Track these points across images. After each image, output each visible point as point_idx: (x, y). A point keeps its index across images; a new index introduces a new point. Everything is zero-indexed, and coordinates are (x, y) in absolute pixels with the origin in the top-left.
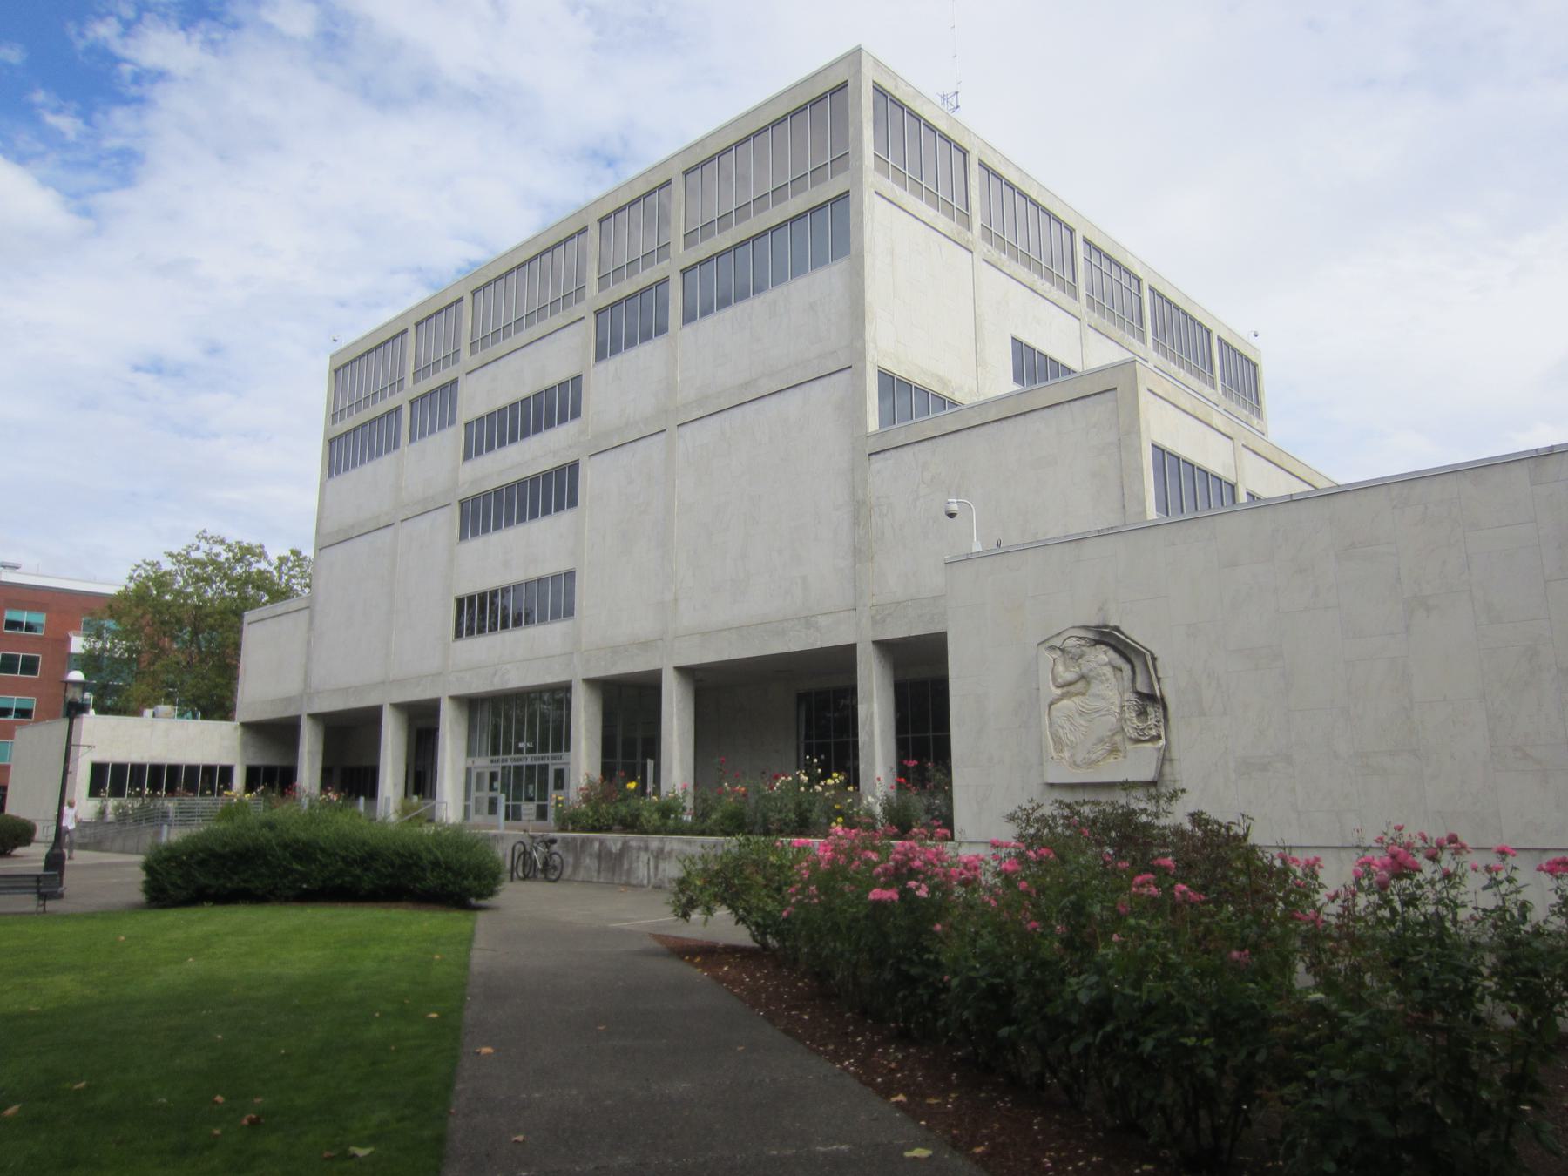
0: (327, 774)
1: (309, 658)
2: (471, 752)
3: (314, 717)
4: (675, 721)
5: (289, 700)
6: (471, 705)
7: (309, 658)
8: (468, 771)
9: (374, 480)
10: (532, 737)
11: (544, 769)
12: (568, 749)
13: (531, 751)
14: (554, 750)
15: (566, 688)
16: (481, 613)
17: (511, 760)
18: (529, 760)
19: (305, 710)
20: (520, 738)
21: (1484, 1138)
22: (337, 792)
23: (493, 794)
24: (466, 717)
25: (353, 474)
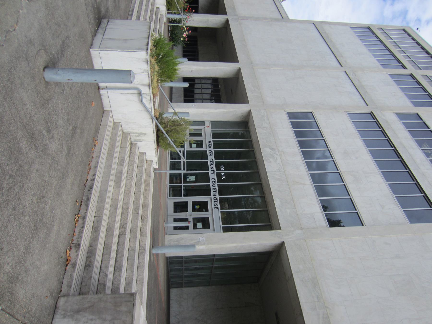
0: (194, 29)
1: (257, 19)
2: (214, 124)
3: (227, 22)
4: (241, 244)
5: (234, 9)
6: (245, 123)
7: (257, 19)
8: (202, 123)
9: (360, 55)
10: (229, 177)
11: (206, 192)
12: (226, 230)
13: (219, 175)
14: (215, 152)
15: (244, 100)
16: (304, 127)
17: (211, 158)
18: (213, 176)
19: (230, 17)
20: (228, 166)
21: (74, 108)
22: (188, 36)
23: (187, 144)
24: (238, 120)
25: (358, 41)
